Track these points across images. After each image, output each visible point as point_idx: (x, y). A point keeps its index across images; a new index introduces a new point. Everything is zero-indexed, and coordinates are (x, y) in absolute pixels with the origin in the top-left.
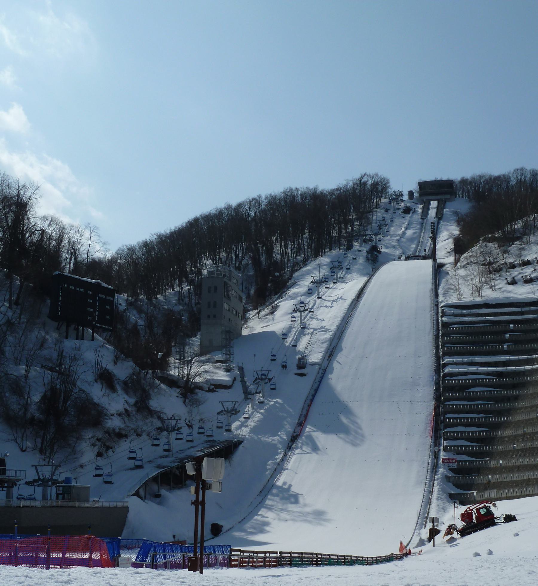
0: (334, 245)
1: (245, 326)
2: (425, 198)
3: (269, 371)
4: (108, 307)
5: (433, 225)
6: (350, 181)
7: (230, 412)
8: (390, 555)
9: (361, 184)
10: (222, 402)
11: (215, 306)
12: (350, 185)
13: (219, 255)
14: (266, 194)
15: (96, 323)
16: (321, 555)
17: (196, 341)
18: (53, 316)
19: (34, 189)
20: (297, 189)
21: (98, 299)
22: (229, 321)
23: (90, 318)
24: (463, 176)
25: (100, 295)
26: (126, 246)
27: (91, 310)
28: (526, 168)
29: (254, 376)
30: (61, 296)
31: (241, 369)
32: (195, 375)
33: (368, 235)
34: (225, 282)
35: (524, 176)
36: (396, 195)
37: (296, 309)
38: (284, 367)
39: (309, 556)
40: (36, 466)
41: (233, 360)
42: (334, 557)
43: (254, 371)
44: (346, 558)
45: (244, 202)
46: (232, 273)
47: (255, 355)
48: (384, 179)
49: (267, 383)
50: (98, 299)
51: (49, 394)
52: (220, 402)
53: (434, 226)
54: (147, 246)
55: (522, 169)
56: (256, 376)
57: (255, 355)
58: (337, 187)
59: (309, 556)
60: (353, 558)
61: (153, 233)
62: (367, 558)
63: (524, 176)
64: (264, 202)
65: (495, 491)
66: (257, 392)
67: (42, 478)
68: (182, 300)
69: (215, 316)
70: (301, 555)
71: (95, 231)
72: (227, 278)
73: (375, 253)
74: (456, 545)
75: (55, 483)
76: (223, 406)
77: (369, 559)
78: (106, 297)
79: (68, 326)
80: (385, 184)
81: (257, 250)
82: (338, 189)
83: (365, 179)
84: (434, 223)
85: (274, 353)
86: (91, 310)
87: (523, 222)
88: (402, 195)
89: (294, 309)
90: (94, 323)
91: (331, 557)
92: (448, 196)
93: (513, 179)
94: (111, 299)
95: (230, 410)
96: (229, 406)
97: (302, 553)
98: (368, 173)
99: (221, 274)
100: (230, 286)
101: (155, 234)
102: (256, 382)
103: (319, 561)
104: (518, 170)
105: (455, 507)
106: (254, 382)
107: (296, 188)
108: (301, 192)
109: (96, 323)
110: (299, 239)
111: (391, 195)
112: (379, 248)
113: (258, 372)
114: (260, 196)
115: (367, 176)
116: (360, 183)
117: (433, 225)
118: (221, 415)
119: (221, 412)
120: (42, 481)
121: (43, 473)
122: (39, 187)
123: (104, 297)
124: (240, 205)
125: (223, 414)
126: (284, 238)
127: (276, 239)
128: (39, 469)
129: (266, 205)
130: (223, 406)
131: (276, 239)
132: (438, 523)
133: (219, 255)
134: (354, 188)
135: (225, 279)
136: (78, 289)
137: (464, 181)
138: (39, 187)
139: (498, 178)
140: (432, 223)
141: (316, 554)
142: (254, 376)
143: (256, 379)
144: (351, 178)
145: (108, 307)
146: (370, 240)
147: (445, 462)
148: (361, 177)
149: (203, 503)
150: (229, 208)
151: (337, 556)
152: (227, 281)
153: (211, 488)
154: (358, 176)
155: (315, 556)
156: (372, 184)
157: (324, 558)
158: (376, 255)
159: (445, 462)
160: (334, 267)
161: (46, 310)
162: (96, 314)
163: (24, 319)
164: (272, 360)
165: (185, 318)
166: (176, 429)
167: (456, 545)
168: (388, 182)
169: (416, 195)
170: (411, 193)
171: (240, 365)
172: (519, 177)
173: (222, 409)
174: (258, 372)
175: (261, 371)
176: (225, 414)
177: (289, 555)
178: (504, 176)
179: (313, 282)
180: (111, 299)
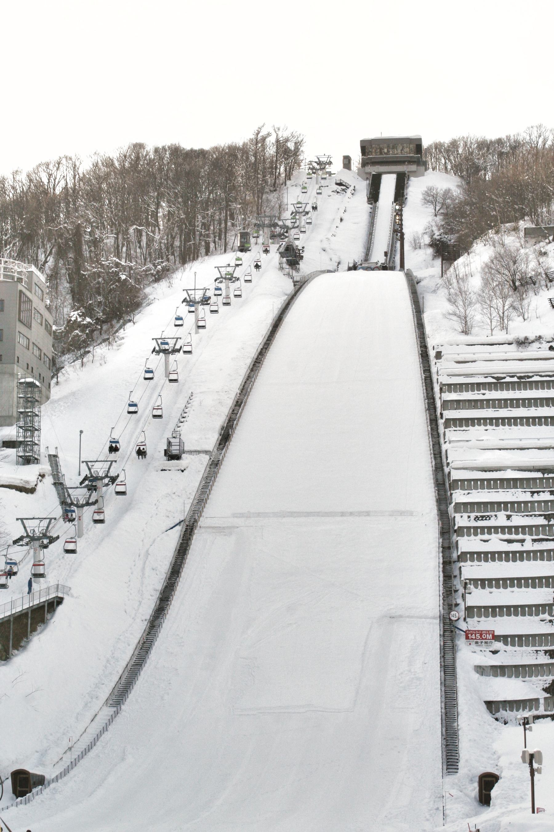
2: (374, 170)
3: (177, 339)
7: (39, 539)
10: (22, 520)
22: (28, 368)
29: (79, 475)
31: (53, 459)
34: (21, 292)
37: (157, 348)
38: (141, 453)
41: (39, 441)
46: (34, 276)
47: (81, 432)
49: (107, 485)
52: (17, 519)
57: (81, 432)
66: (90, 502)
72: (23, 284)
76: (25, 527)
85: (135, 400)
89: (155, 348)
92: (413, 167)
95: (38, 534)
99: (13, 278)
100: (30, 301)
106: (81, 483)
112: (299, 250)
118: (22, 545)
119: (21, 539)
125: (24, 544)
130: (25, 527)
135: (20, 287)
143: (85, 479)
147: (472, 639)
152: (24, 290)
153: (95, 523)
159: (472, 639)
160: (222, 277)
164: (129, 413)
171: (53, 452)
173: (23, 533)
174: (25, 521)
175: (195, 289)
176: (27, 544)
179: (187, 302)
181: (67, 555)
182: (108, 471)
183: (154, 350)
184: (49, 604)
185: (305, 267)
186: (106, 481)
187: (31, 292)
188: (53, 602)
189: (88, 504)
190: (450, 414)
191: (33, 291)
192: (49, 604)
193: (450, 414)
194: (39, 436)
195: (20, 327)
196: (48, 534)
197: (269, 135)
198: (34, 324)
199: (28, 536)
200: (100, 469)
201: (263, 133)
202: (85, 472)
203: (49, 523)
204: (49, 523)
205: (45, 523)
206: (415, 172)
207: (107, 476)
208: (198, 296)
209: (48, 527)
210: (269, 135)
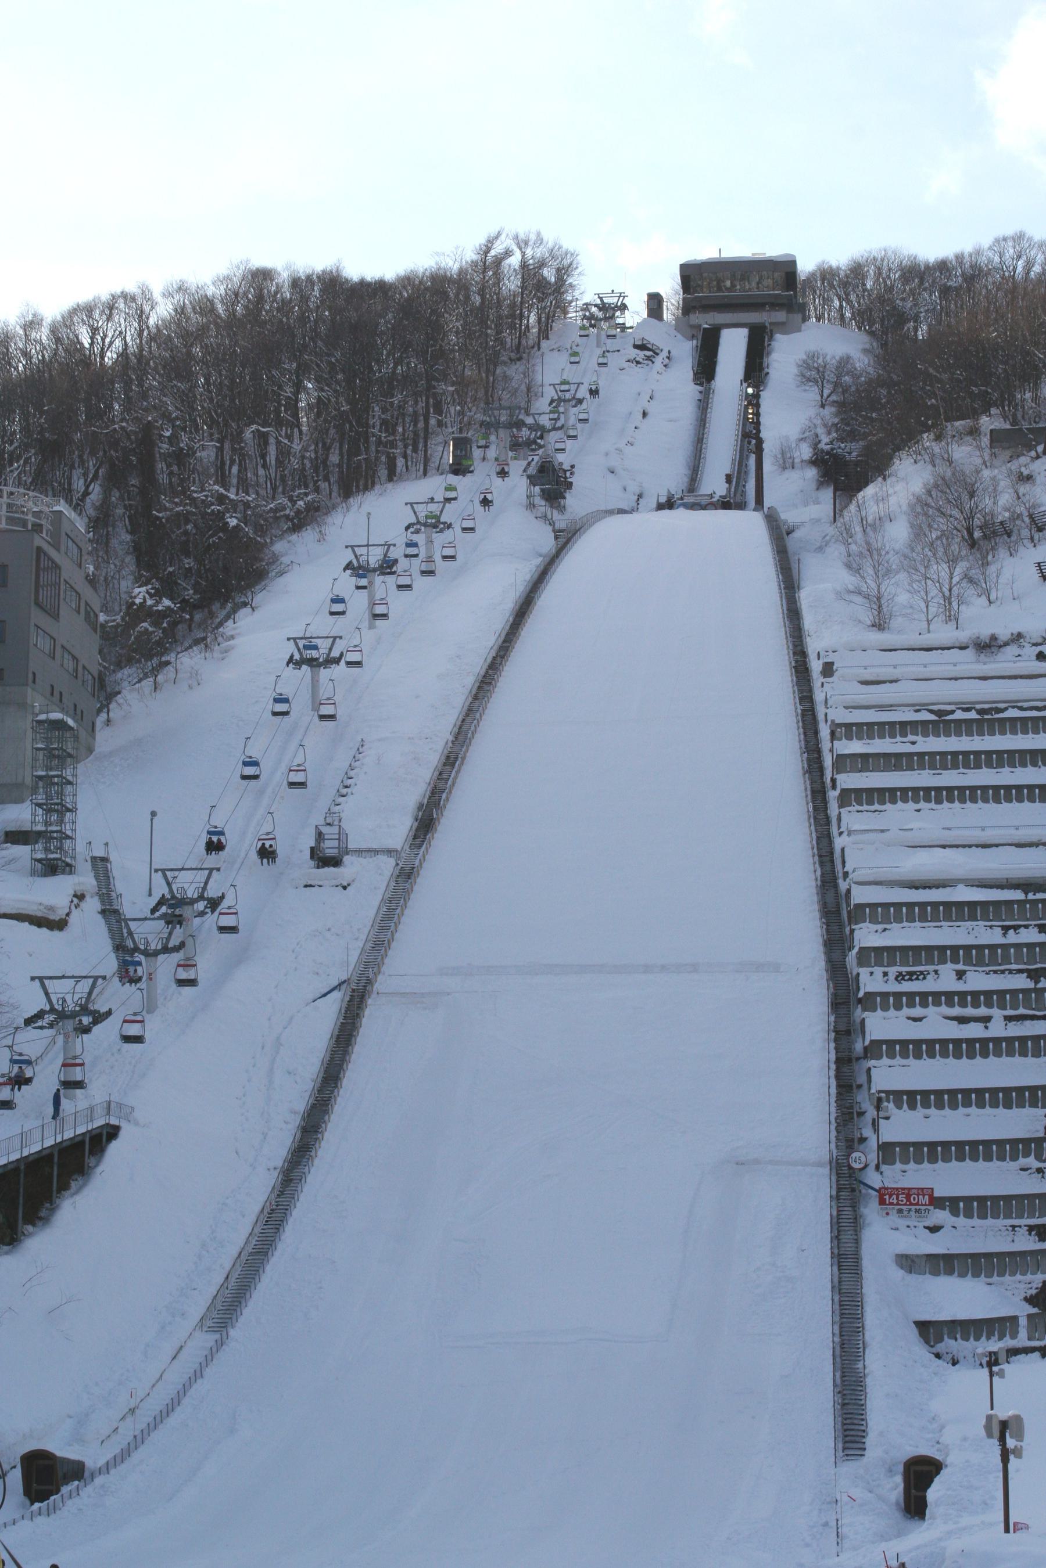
1: (103, 716)
2: (705, 320)
7: (73, 1015)
10: (41, 979)
22: (52, 694)
29: (150, 895)
31: (101, 865)
34: (39, 549)
36: (603, 307)
37: (297, 657)
38: (266, 854)
41: (74, 830)
47: (154, 814)
49: (202, 914)
57: (154, 814)
64: (162, 311)
66: (170, 945)
72: (44, 535)
76: (47, 994)
88: (623, 307)
89: (292, 656)
92: (780, 316)
95: (71, 1006)
99: (24, 523)
104: (1005, 239)
106: (154, 910)
110: (337, 360)
111: (587, 306)
112: (565, 471)
113: (46, 982)
118: (41, 1028)
119: (40, 1015)
130: (47, 994)
135: (38, 541)
142: (150, 895)
147: (891, 1204)
148: (489, 241)
152: (46, 547)
160: (418, 522)
169: (670, 312)
170: (655, 303)
171: (99, 853)
173: (42, 1004)
174: (46, 982)
176: (51, 1026)
182: (204, 888)
183: (291, 660)
185: (576, 503)
186: (201, 906)
187: (58, 550)
188: (100, 1135)
189: (166, 950)
190: (850, 780)
191: (63, 548)
192: (92, 1139)
193: (850, 780)
196: (91, 1007)
197: (508, 253)
198: (64, 611)
199: (53, 1010)
200: (188, 884)
201: (497, 249)
202: (161, 889)
203: (93, 986)
204: (93, 986)
205: (85, 986)
206: (782, 325)
207: (201, 897)
208: (374, 557)
209: (90, 993)
210: (508, 253)
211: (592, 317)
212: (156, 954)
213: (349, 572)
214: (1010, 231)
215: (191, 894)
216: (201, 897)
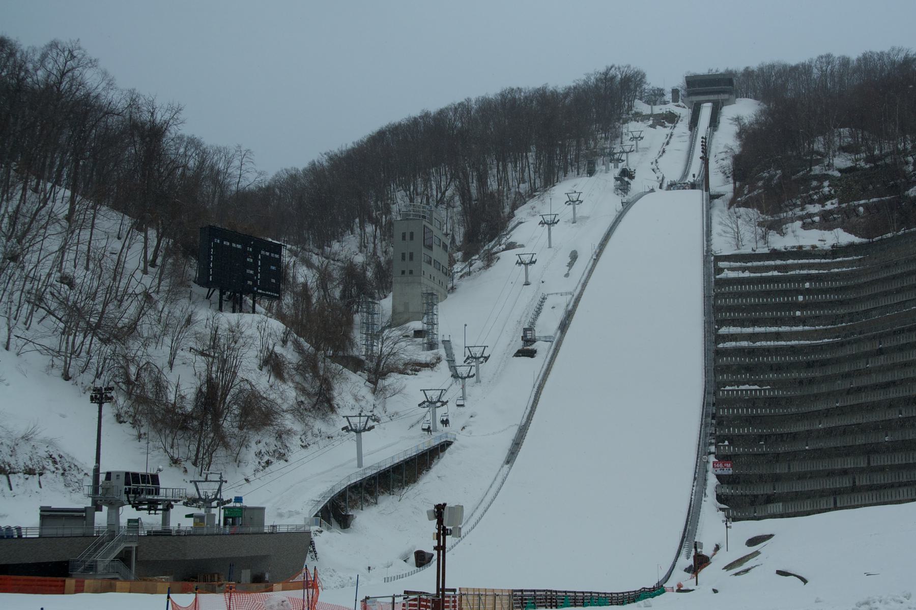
0: (570, 168)
2: (696, 99)
4: (273, 268)
5: (704, 140)
6: (592, 75)
8: (640, 590)
9: (606, 79)
10: (424, 390)
11: (411, 258)
12: (592, 81)
13: (414, 183)
14: (477, 97)
15: (257, 289)
16: (556, 592)
17: (386, 304)
18: (202, 281)
19: (174, 111)
20: (520, 90)
21: (260, 257)
23: (250, 283)
24: (747, 66)
25: (263, 252)
26: (286, 170)
27: (252, 272)
28: (834, 55)
30: (213, 255)
31: (446, 343)
32: (388, 355)
33: (616, 153)
34: (424, 226)
35: (830, 66)
37: (520, 261)
39: (542, 593)
40: (195, 482)
42: (571, 594)
43: (465, 347)
44: (585, 594)
45: (446, 108)
47: (466, 325)
48: (637, 73)
49: (482, 362)
50: (260, 257)
51: (204, 389)
52: (421, 390)
53: (706, 142)
54: (314, 171)
55: (828, 56)
56: (468, 353)
57: (466, 325)
58: (575, 84)
59: (542, 593)
60: (593, 595)
61: (323, 153)
62: (611, 594)
63: (830, 66)
65: (781, 504)
66: (470, 375)
67: (203, 497)
68: (365, 247)
69: (411, 272)
70: (533, 593)
71: (248, 156)
73: (626, 179)
74: (747, 571)
75: (221, 503)
76: (426, 395)
77: (613, 595)
78: (270, 255)
79: (222, 294)
80: (639, 80)
81: (466, 176)
82: (575, 88)
83: (612, 72)
84: (706, 139)
86: (252, 272)
87: (825, 139)
88: (663, 95)
89: (518, 261)
90: (255, 289)
91: (568, 594)
92: (726, 96)
93: (815, 71)
94: (277, 256)
96: (434, 395)
97: (534, 591)
98: (616, 66)
101: (325, 154)
102: (468, 361)
103: (554, 602)
105: (727, 527)
106: (465, 362)
107: (518, 88)
108: (525, 93)
109: (257, 289)
114: (469, 100)
115: (616, 69)
116: (605, 78)
117: (704, 140)
118: (424, 407)
119: (424, 402)
120: (204, 500)
121: (205, 491)
122: (180, 110)
123: (268, 254)
124: (441, 112)
126: (502, 159)
127: (491, 160)
128: (200, 485)
129: (477, 111)
130: (426, 395)
131: (491, 160)
132: (702, 549)
133: (414, 183)
134: (596, 86)
135: (424, 223)
136: (234, 245)
137: (748, 73)
138: (180, 110)
139: (795, 69)
140: (702, 138)
141: (551, 591)
143: (468, 358)
144: (591, 71)
145: (273, 268)
146: (619, 160)
148: (607, 70)
149: (444, 548)
150: (426, 115)
151: (575, 592)
154: (602, 69)
155: (549, 593)
156: (621, 79)
157: (559, 596)
158: (627, 182)
161: (193, 273)
162: (257, 277)
163: (165, 286)
165: (369, 274)
166: (367, 428)
167: (747, 571)
168: (644, 76)
169: (682, 92)
170: (675, 92)
171: (447, 338)
172: (824, 68)
174: (426, 391)
177: (520, 593)
178: (803, 65)
179: (543, 224)
180: (277, 256)
181: (459, 408)
182: (483, 353)
183: (517, 262)
184: (441, 446)
185: (636, 186)
186: (482, 359)
187: (432, 224)
188: (444, 445)
189: (469, 377)
190: (416, 603)
191: (434, 224)
192: (441, 446)
193: (416, 603)
194: (437, 329)
195: (424, 250)
196: (441, 400)
198: (434, 247)
199: (428, 401)
203: (442, 392)
204: (442, 392)
205: (439, 392)
206: (727, 100)
207: (482, 357)
209: (440, 395)
211: (655, 93)
212: (465, 378)
213: (541, 225)
214: (824, 53)
215: (478, 355)
216: (482, 357)
